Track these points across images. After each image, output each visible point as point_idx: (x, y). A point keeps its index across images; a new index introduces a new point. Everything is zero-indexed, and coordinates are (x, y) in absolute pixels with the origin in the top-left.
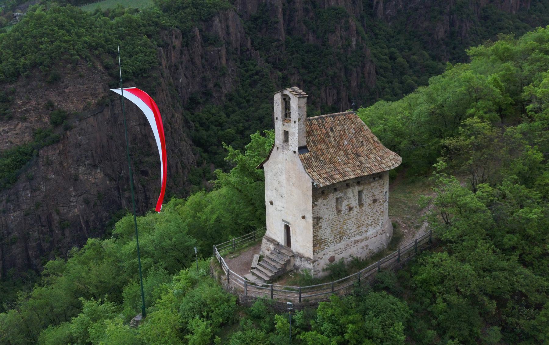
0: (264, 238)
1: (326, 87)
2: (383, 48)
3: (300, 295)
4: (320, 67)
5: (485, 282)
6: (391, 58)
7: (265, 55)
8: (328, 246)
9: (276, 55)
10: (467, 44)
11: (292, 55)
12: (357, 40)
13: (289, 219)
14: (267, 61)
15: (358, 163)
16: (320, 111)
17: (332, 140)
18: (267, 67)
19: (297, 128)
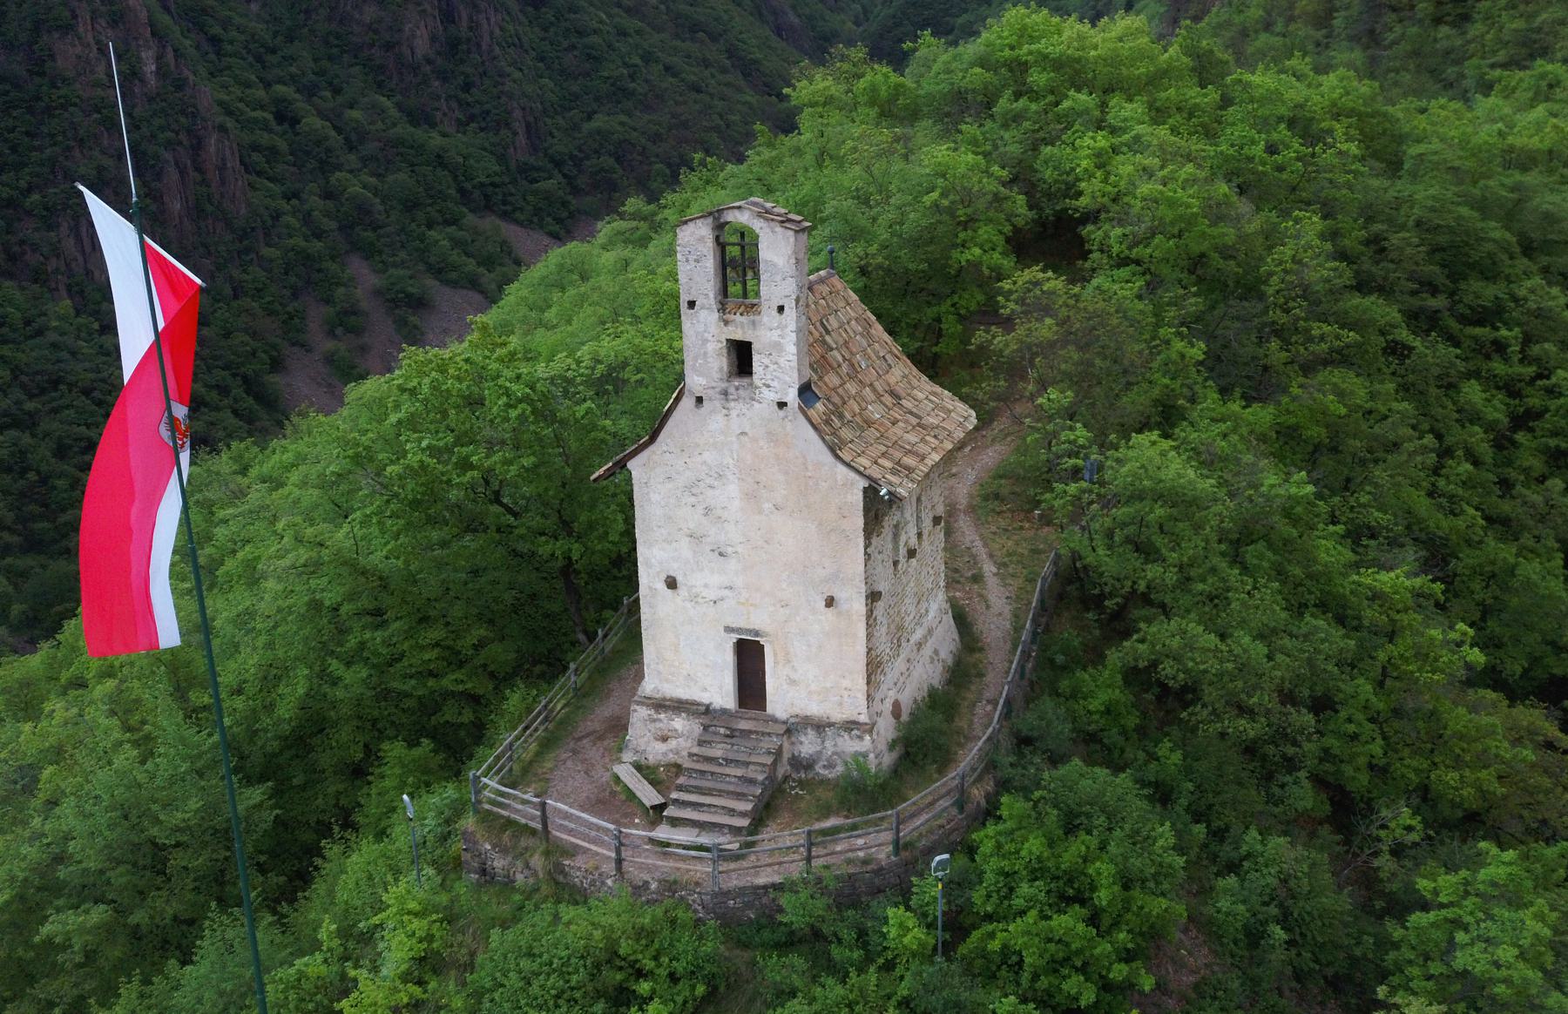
0: (638, 703)
2: (248, 85)
4: (40, 149)
6: (280, 117)
10: (500, 76)
12: (159, 58)
13: (758, 620)
16: (68, 302)
19: (792, 326)
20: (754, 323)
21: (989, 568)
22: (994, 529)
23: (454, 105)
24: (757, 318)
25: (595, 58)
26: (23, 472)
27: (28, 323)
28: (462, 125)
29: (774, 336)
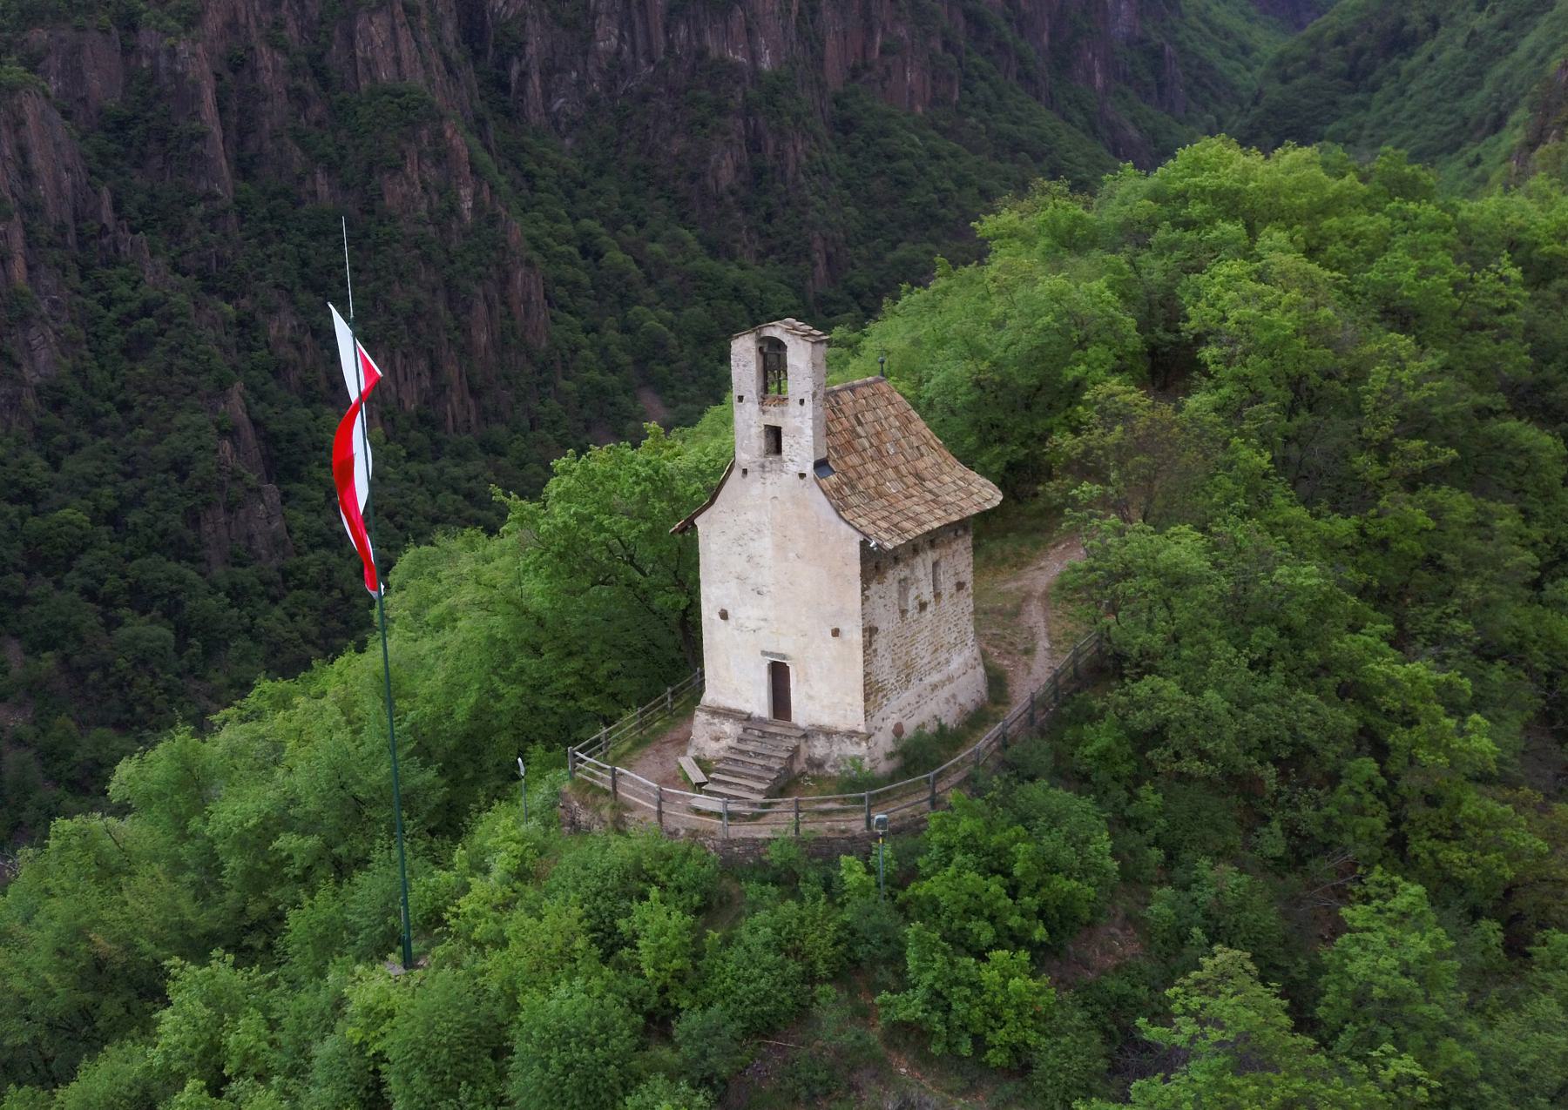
2: (556, 219)
6: (585, 252)
9: (206, 245)
11: (262, 245)
12: (476, 195)
13: (786, 646)
14: (176, 268)
15: (929, 497)
17: (867, 445)
18: (180, 289)
21: (1043, 643)
22: (1060, 613)
23: (754, 236)
25: (904, 184)
26: (330, 588)
28: (761, 256)
29: (797, 422)
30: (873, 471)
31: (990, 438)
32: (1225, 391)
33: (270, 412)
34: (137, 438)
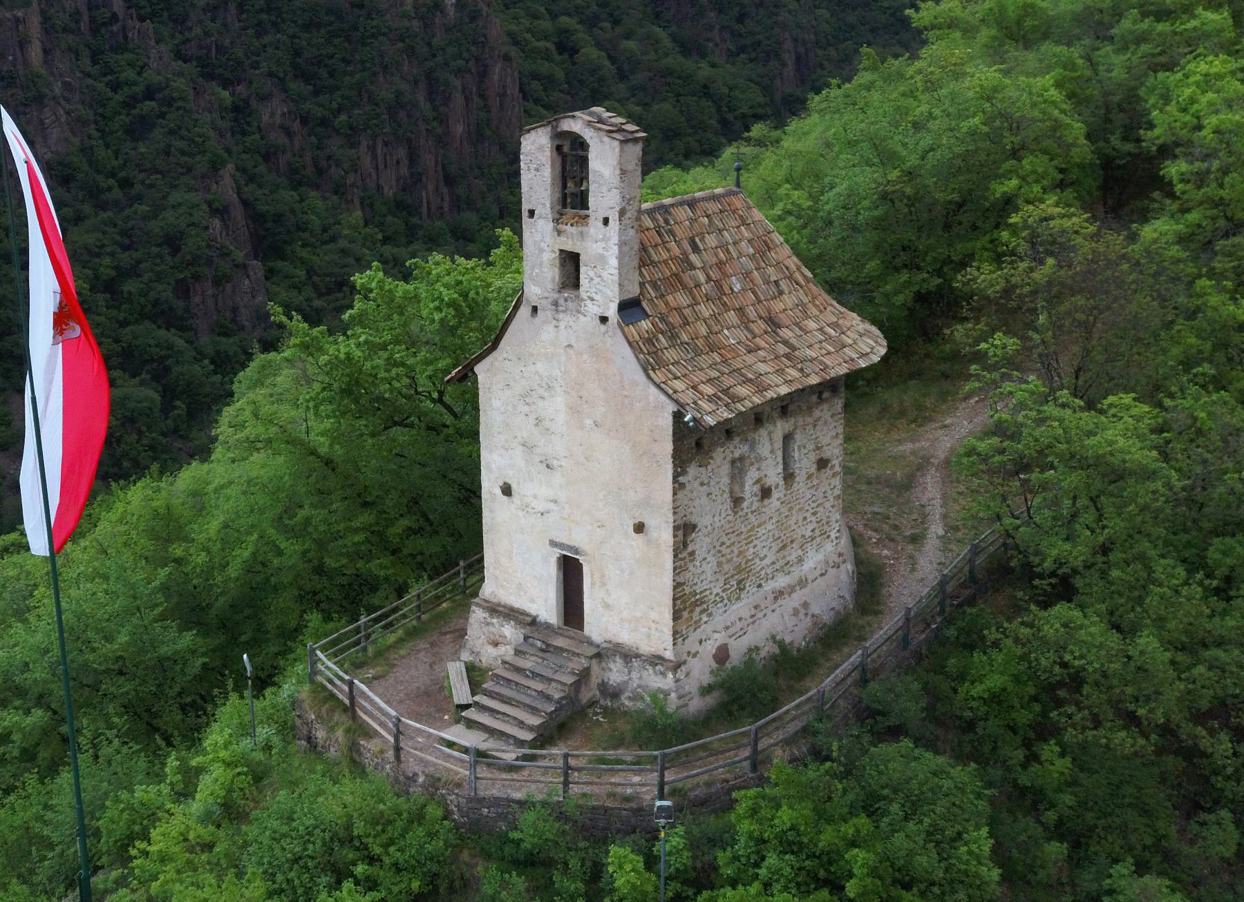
0: (478, 605)
1: (374, 137)
2: (536, 16)
3: (662, 776)
4: (352, 74)
5: (1194, 682)
6: (561, 48)
7: (173, 36)
8: (710, 615)
9: (207, 34)
11: (259, 35)
13: (579, 537)
14: (179, 55)
15: (782, 349)
16: (359, 213)
17: (702, 277)
18: (181, 74)
19: (615, 239)
20: (582, 234)
22: (962, 488)
23: (727, 35)
24: (585, 229)
27: (325, 230)
28: (732, 55)
30: (707, 314)
31: (898, 262)
32: (1193, 217)
33: (259, 192)
34: (135, 213)
